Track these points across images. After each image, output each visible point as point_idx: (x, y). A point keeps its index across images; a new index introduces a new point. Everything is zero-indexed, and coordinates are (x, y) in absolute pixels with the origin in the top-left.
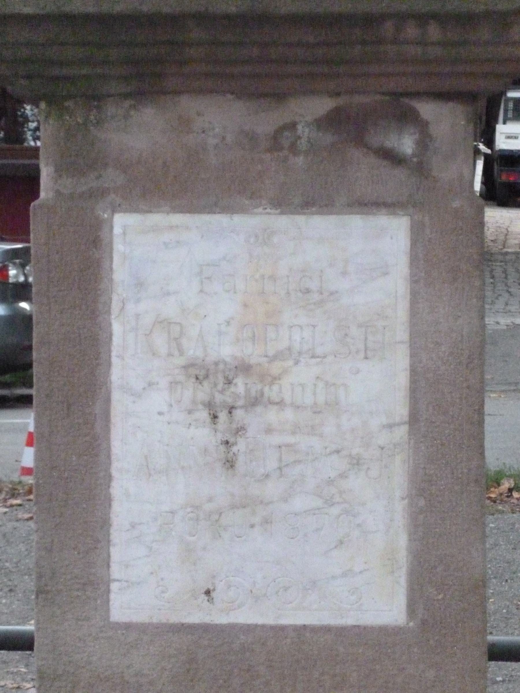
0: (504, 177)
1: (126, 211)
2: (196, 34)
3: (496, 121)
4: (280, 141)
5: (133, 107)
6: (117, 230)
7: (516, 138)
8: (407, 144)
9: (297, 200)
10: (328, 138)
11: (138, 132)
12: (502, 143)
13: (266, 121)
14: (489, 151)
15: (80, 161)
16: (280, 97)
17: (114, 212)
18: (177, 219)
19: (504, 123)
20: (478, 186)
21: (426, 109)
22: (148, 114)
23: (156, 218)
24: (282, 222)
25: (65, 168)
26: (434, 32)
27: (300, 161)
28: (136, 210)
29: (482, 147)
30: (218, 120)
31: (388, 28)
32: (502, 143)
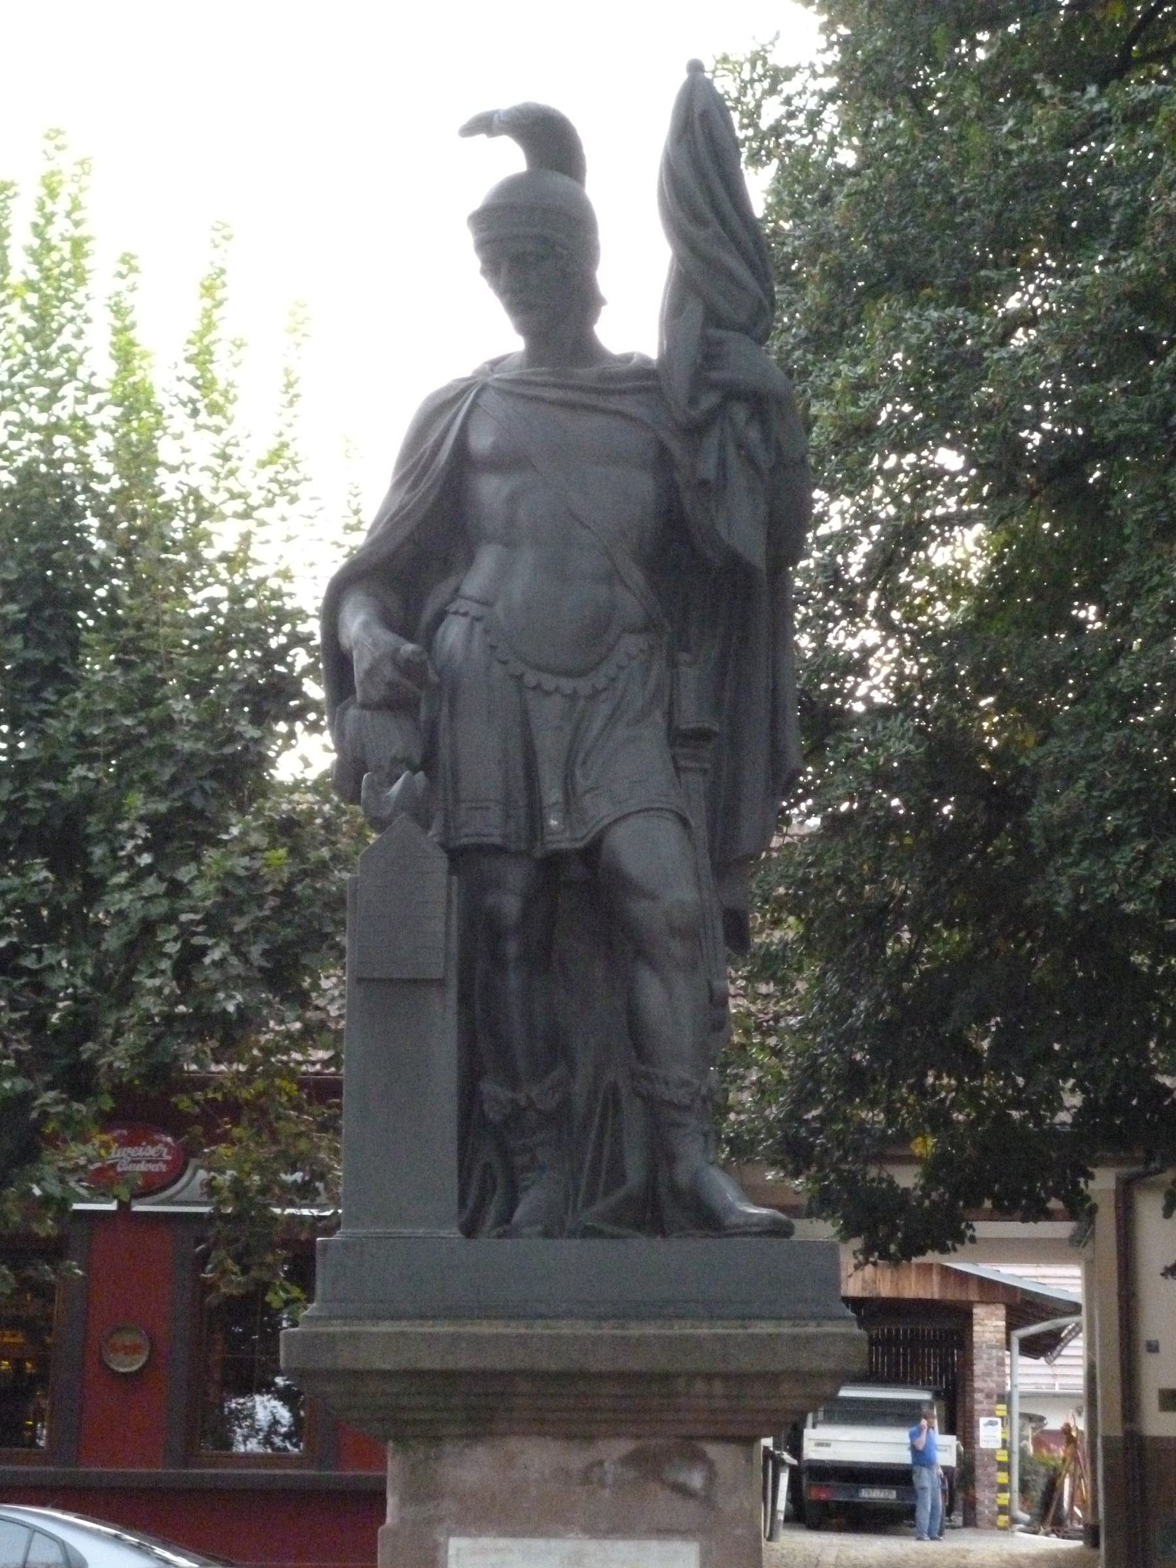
0: (815, 1493)
1: (460, 1535)
2: (524, 1387)
3: (804, 1426)
4: (589, 1476)
5: (467, 1446)
6: (451, 1552)
7: (828, 1445)
8: (696, 1480)
9: (604, 1526)
10: (631, 1474)
11: (471, 1467)
12: (811, 1452)
13: (577, 1459)
14: (795, 1462)
15: (423, 1491)
16: (590, 1438)
17: (449, 1536)
18: (503, 1542)
19: (814, 1426)
20: (782, 1504)
21: (713, 1451)
22: (480, 1452)
23: (485, 1542)
24: (591, 1546)
25: (411, 1497)
26: (718, 1387)
27: (607, 1493)
28: (469, 1535)
29: (787, 1457)
30: (538, 1458)
31: (681, 1384)
32: (811, 1452)
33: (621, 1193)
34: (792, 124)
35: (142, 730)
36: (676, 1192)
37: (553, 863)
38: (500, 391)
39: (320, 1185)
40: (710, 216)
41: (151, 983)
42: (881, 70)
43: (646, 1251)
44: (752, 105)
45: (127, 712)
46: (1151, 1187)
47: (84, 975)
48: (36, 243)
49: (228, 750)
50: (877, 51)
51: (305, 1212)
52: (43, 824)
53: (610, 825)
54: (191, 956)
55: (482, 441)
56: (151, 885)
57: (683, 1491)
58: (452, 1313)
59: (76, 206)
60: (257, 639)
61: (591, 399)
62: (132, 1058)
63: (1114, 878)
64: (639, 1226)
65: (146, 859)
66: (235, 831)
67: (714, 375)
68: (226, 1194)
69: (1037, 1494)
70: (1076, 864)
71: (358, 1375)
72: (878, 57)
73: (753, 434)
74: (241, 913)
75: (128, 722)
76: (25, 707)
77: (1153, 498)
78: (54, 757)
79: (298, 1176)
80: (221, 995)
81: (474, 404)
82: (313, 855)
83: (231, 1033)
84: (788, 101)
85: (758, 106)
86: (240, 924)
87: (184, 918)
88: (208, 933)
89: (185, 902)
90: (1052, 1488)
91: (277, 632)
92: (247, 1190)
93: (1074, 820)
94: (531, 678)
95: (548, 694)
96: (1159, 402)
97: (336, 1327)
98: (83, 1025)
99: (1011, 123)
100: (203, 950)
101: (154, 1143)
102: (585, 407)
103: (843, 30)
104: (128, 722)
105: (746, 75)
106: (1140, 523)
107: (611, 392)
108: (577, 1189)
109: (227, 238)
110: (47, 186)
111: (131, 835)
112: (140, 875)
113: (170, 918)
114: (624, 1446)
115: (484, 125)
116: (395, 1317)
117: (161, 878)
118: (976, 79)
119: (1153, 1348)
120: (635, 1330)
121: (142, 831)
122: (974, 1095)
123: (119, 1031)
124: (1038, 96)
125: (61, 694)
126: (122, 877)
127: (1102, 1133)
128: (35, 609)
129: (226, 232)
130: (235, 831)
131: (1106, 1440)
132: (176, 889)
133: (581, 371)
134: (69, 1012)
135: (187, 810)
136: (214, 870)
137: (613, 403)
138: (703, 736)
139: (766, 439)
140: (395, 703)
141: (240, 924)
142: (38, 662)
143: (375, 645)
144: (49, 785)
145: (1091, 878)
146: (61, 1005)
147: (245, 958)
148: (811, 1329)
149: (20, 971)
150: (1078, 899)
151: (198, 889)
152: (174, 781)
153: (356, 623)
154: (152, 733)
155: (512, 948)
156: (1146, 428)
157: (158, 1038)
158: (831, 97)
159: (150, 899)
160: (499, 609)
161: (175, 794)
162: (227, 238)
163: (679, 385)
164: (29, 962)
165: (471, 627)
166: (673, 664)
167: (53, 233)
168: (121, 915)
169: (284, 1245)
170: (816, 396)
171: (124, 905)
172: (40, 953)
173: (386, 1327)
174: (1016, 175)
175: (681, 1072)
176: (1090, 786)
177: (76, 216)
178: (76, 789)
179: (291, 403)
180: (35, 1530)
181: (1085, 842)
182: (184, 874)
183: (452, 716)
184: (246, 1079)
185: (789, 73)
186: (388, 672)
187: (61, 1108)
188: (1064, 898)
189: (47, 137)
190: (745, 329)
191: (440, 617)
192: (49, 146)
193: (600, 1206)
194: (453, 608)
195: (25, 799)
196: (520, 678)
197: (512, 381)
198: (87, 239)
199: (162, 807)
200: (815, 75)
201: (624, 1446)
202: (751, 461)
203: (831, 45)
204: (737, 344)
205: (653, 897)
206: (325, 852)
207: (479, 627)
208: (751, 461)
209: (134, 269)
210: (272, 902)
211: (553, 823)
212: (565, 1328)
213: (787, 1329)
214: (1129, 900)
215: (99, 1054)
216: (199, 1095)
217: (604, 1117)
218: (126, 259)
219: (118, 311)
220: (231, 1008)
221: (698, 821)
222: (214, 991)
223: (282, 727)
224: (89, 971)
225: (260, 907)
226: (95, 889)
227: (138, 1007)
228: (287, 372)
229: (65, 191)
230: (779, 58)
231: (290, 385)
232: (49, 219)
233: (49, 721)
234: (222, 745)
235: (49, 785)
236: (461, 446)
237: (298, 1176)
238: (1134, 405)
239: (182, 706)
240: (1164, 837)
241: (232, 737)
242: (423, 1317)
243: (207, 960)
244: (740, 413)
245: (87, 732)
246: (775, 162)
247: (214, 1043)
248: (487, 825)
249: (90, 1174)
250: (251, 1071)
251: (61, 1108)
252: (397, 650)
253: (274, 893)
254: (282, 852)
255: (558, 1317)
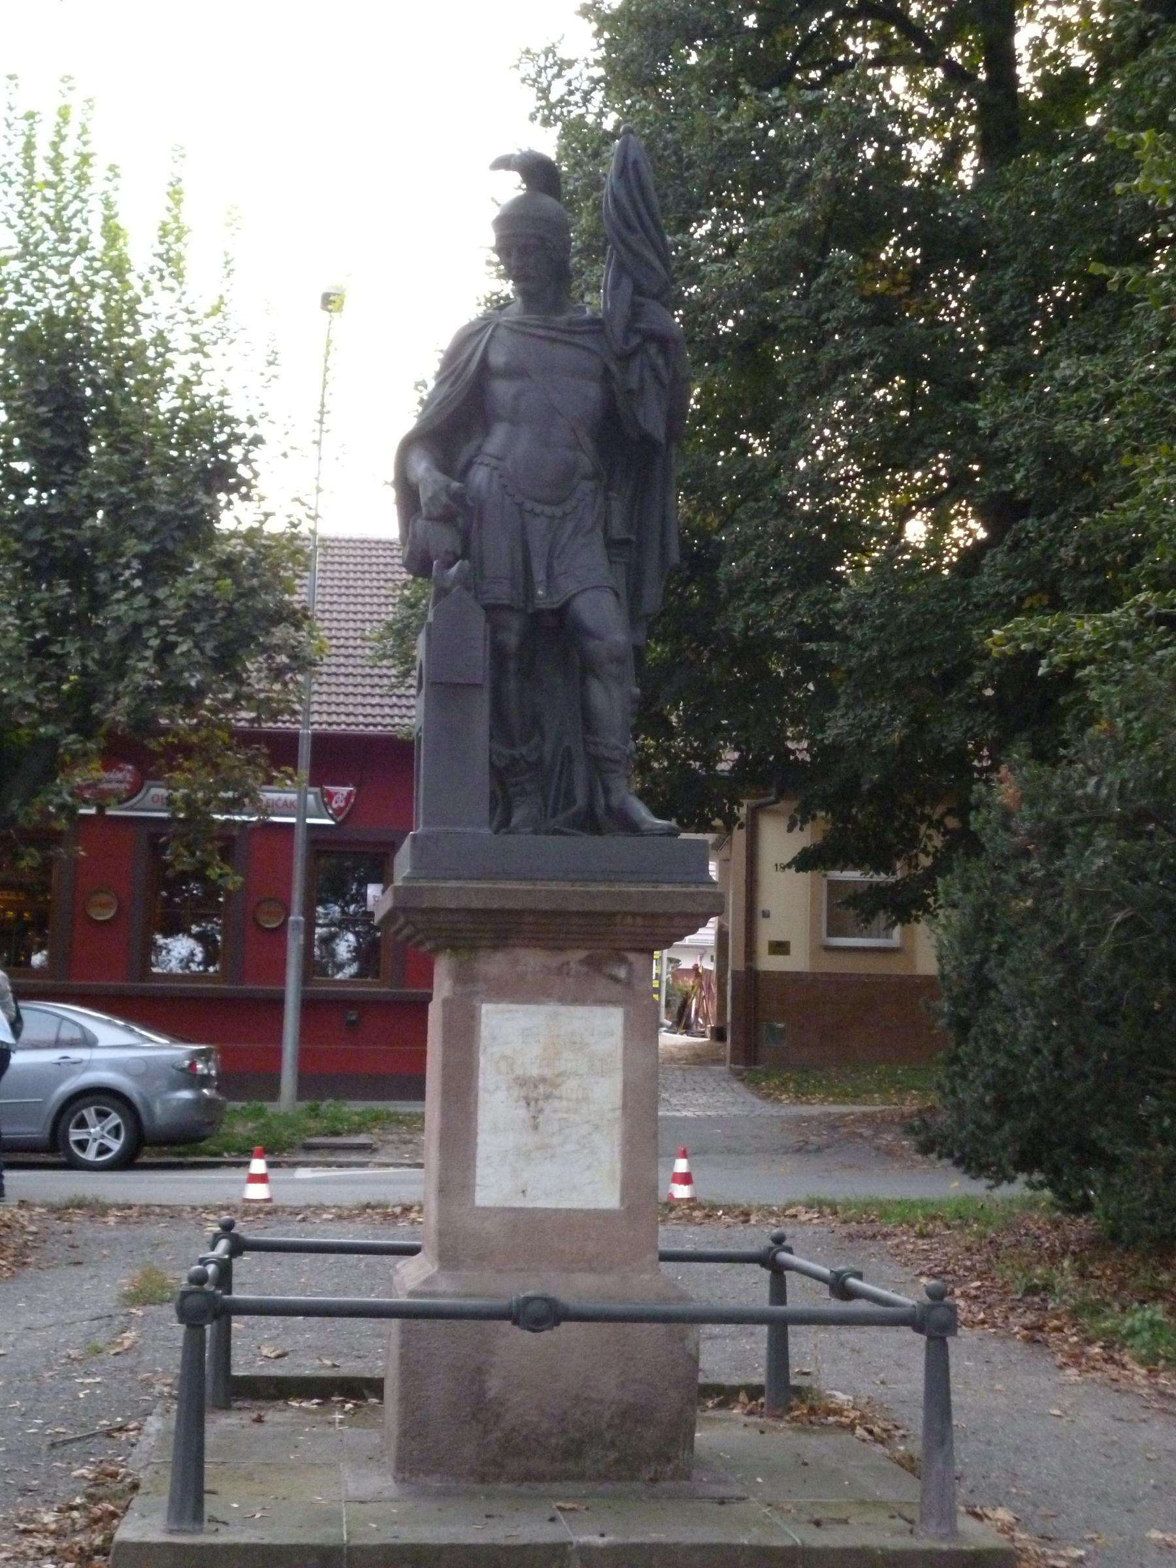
1: (490, 1002)
4: (561, 970)
8: (622, 973)
10: (584, 969)
13: (555, 960)
16: (562, 949)
21: (632, 957)
22: (499, 956)
23: (502, 1006)
24: (563, 1009)
26: (639, 921)
30: (532, 960)
31: (618, 919)
33: (574, 810)
34: (572, 99)
35: (133, 495)
36: (609, 809)
37: (538, 615)
38: (506, 328)
39: (246, 800)
40: (636, 224)
41: (141, 665)
42: (634, 67)
43: (588, 842)
44: (545, 85)
45: (123, 483)
46: (776, 813)
47: (93, 659)
48: (52, 154)
49: (190, 511)
50: (633, 54)
51: (237, 818)
52: (64, 556)
53: (575, 595)
54: (167, 648)
55: (498, 359)
56: (140, 600)
57: (615, 979)
58: (493, 878)
59: (85, 131)
60: (208, 436)
61: (560, 336)
62: (128, 715)
63: (771, 615)
64: (582, 828)
65: (137, 583)
66: (197, 566)
67: (637, 325)
68: (180, 804)
69: (675, 1009)
70: (746, 605)
71: (433, 911)
72: (633, 58)
73: (660, 362)
74: (198, 621)
75: (124, 490)
76: (52, 478)
77: (806, 369)
78: (71, 511)
79: (230, 794)
80: (186, 675)
81: (492, 336)
82: (246, 584)
83: (191, 699)
84: (569, 83)
85: (550, 85)
86: (199, 628)
87: (162, 623)
88: (178, 634)
89: (161, 613)
90: (685, 1005)
91: (221, 432)
92: (196, 801)
93: (747, 576)
94: (528, 505)
95: (537, 515)
96: (814, 306)
97: (424, 884)
98: (88, 692)
99: (723, 110)
100: (175, 645)
101: (121, 770)
102: (560, 341)
103: (607, 35)
104: (124, 490)
105: (542, 64)
106: (798, 385)
107: (575, 333)
108: (546, 806)
109: (183, 156)
110: (61, 116)
111: (127, 566)
112: (136, 592)
113: (153, 622)
114: (582, 954)
115: (504, 163)
116: (457, 878)
117: (147, 596)
118: (699, 78)
119: (766, 915)
120: (593, 888)
121: (136, 565)
122: (666, 752)
123: (117, 697)
124: (740, 95)
125: (77, 469)
126: (120, 594)
127: (749, 776)
128: (57, 410)
129: (182, 152)
130: (197, 566)
131: (734, 973)
132: (155, 603)
133: (558, 319)
134: (75, 685)
135: (163, 551)
136: (183, 592)
137: (577, 339)
138: (626, 542)
139: (667, 364)
140: (446, 518)
141: (199, 628)
142: (59, 446)
143: (435, 481)
144: (69, 531)
145: (757, 614)
146: (72, 678)
147: (202, 652)
148: (692, 889)
149: (51, 655)
150: (747, 628)
151: (172, 604)
152: (154, 532)
153: (421, 467)
154: (139, 499)
155: (512, 666)
156: (805, 323)
157: (143, 701)
158: (595, 82)
159: (138, 610)
160: (508, 464)
161: (156, 540)
162: (183, 156)
163: (617, 328)
164: (56, 649)
165: (491, 476)
166: (607, 499)
167: (64, 149)
168: (118, 620)
169: (220, 838)
170: (587, 289)
171: (120, 613)
172: (63, 643)
173: (452, 884)
174: (725, 145)
175: (614, 741)
176: (758, 555)
177: (84, 138)
178: (88, 534)
179: (228, 275)
180: (63, 1018)
181: (754, 591)
182: (161, 593)
183: (480, 527)
184: (195, 729)
185: (570, 64)
186: (444, 499)
187: (79, 746)
188: (738, 627)
189: (62, 81)
190: (656, 297)
191: (469, 465)
192: (64, 87)
193: (561, 817)
194: (479, 460)
195: (53, 539)
196: (520, 505)
197: (518, 323)
198: (91, 155)
199: (147, 548)
200: (587, 65)
201: (582, 954)
202: (658, 378)
203: (600, 46)
204: (652, 306)
205: (601, 639)
206: (255, 582)
207: (496, 473)
208: (658, 378)
209: (117, 175)
210: (221, 614)
211: (540, 592)
212: (553, 886)
213: (678, 889)
214: (781, 629)
215: (104, 712)
216: (162, 739)
217: (563, 764)
218: (112, 168)
219: (108, 205)
220: (193, 683)
221: (623, 594)
222: (182, 671)
223: (222, 497)
224: (97, 656)
225: (213, 617)
226: (98, 601)
227: (132, 681)
228: (226, 254)
229: (75, 118)
230: (563, 53)
231: (227, 263)
232: (63, 138)
233: (69, 488)
234: (187, 507)
235: (69, 531)
236: (484, 361)
237: (230, 794)
238: (799, 307)
239: (162, 482)
240: (804, 590)
241: (193, 503)
242: (472, 878)
243: (178, 651)
244: (653, 349)
245: (96, 496)
246: (559, 124)
247: (180, 706)
248: (502, 593)
249: (93, 787)
250: (199, 723)
251: (79, 746)
252: (448, 486)
253: (224, 608)
254: (229, 581)
255: (550, 880)
